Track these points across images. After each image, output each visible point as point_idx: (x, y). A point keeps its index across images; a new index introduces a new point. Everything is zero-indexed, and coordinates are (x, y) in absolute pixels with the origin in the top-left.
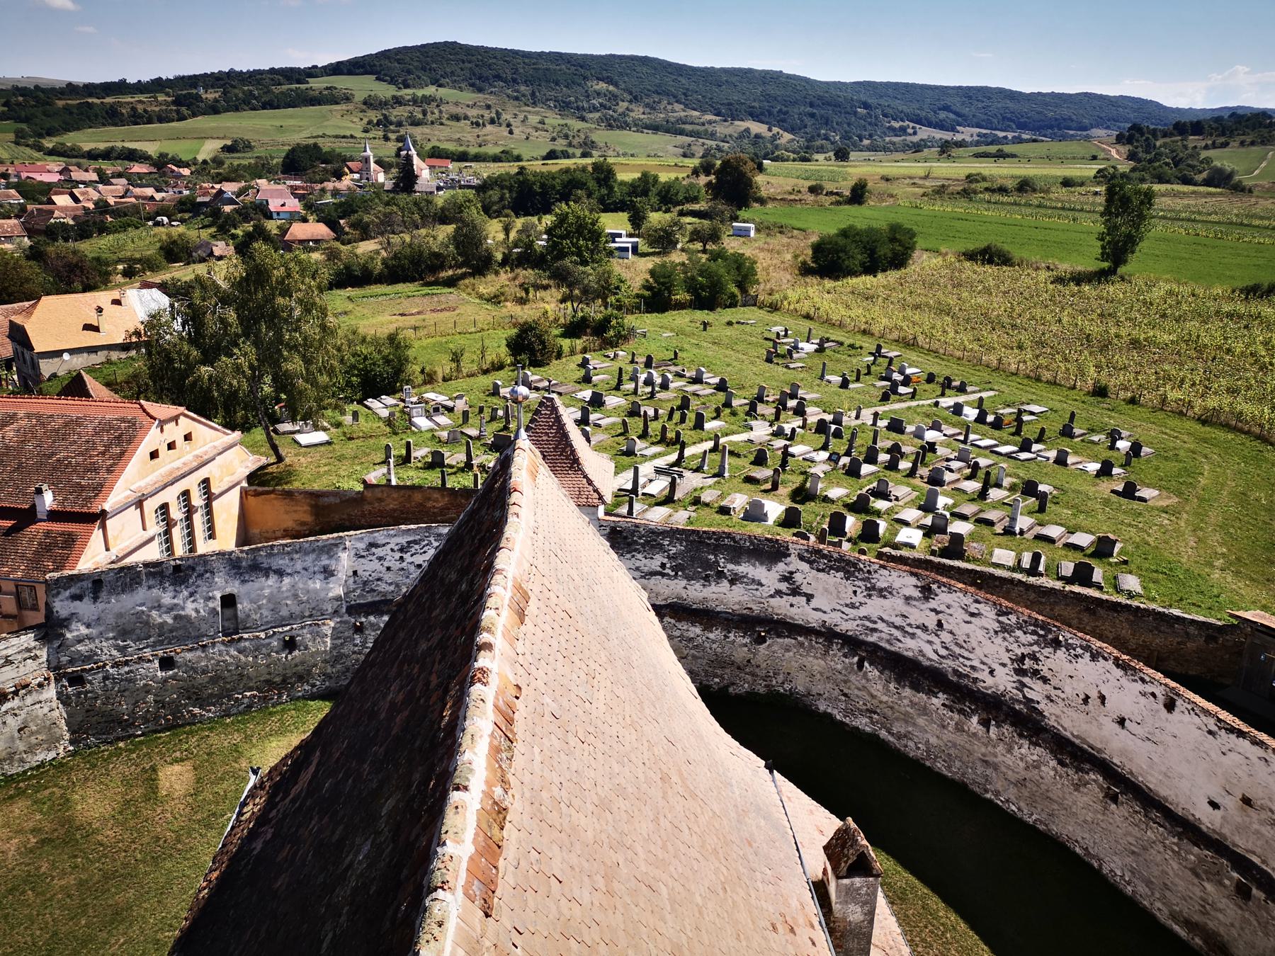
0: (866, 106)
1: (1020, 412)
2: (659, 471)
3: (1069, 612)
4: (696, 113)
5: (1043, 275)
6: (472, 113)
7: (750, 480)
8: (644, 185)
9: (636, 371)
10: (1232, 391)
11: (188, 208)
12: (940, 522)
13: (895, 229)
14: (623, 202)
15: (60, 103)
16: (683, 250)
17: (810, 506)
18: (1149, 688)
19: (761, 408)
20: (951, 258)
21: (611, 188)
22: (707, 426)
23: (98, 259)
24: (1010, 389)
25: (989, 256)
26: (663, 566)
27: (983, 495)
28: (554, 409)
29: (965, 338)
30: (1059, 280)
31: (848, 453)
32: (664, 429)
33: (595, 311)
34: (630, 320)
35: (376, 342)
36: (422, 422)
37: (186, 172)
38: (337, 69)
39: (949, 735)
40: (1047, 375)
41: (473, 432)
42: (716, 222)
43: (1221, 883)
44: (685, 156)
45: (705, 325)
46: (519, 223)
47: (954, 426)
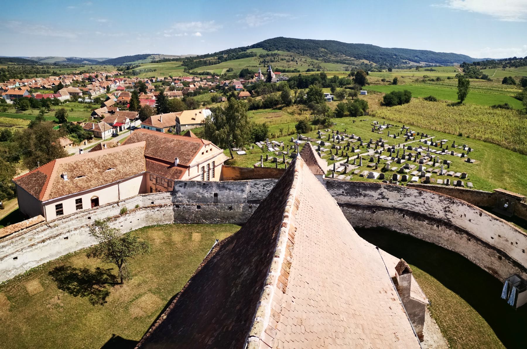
0: (396, 55)
1: (441, 142)
2: (341, 165)
3: (456, 194)
4: (349, 57)
5: (444, 104)
6: (287, 58)
7: (369, 166)
8: (335, 80)
9: (334, 135)
10: (491, 133)
11: (218, 87)
12: (423, 174)
13: (406, 91)
14: (329, 85)
15: (195, 61)
16: (346, 99)
17: (387, 173)
18: (476, 211)
19: (371, 145)
20: (421, 100)
21: (325, 81)
22: (356, 151)
23: (197, 101)
24: (439, 136)
25: (431, 99)
26: (343, 192)
27: (434, 165)
28: (309, 146)
29: (426, 122)
30: (448, 105)
31: (397, 157)
32: (343, 152)
33: (321, 117)
34: (332, 120)
35: (260, 126)
36: (271, 149)
37: (218, 78)
38: (253, 46)
39: (429, 231)
40: (447, 131)
41: (285, 153)
42: (356, 91)
43: (495, 257)
44: (346, 70)
45: (354, 121)
46: (299, 91)
47: (425, 147)
